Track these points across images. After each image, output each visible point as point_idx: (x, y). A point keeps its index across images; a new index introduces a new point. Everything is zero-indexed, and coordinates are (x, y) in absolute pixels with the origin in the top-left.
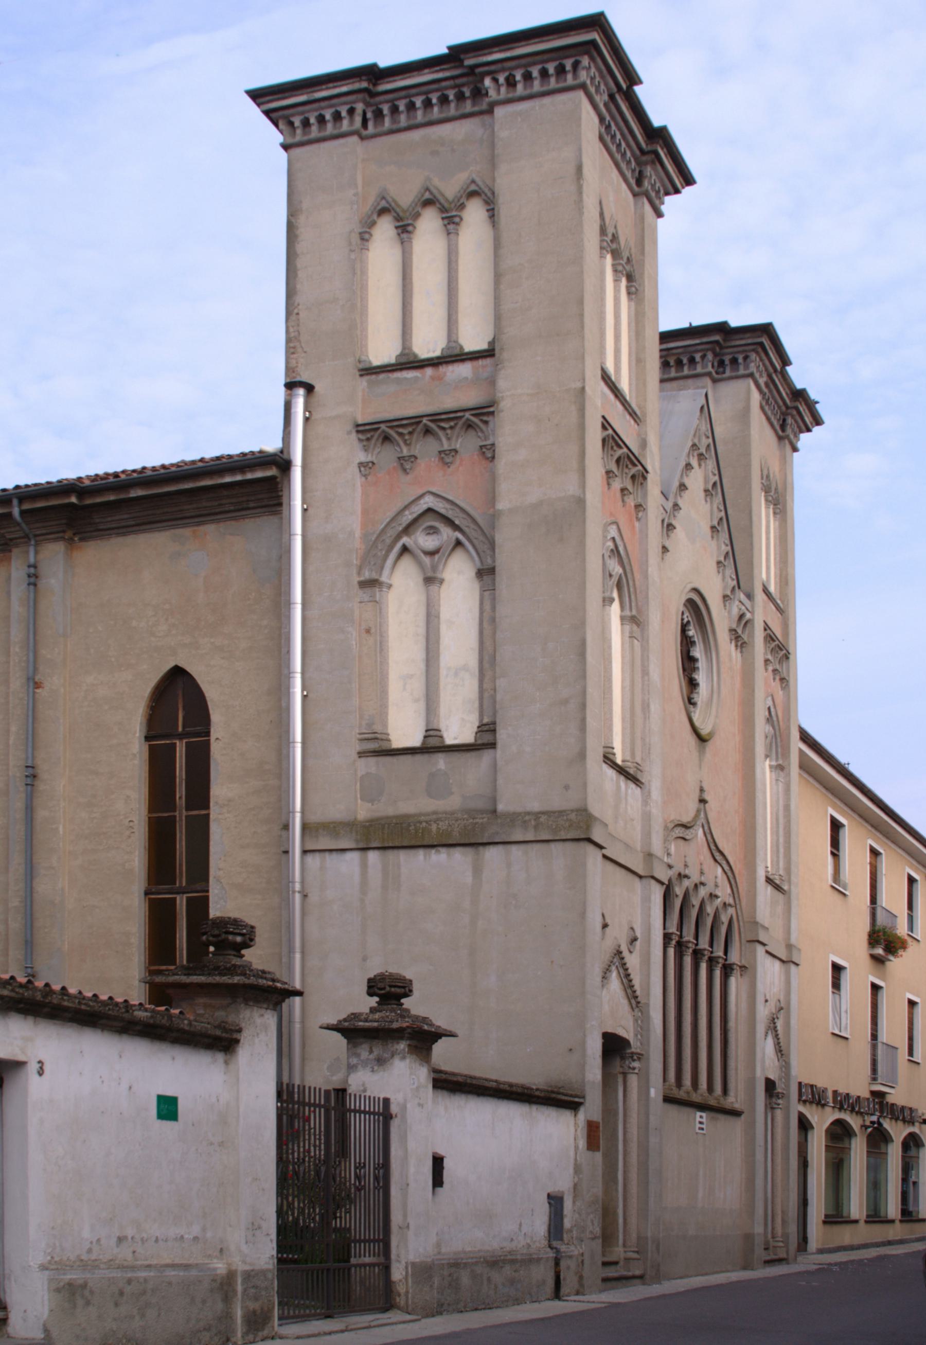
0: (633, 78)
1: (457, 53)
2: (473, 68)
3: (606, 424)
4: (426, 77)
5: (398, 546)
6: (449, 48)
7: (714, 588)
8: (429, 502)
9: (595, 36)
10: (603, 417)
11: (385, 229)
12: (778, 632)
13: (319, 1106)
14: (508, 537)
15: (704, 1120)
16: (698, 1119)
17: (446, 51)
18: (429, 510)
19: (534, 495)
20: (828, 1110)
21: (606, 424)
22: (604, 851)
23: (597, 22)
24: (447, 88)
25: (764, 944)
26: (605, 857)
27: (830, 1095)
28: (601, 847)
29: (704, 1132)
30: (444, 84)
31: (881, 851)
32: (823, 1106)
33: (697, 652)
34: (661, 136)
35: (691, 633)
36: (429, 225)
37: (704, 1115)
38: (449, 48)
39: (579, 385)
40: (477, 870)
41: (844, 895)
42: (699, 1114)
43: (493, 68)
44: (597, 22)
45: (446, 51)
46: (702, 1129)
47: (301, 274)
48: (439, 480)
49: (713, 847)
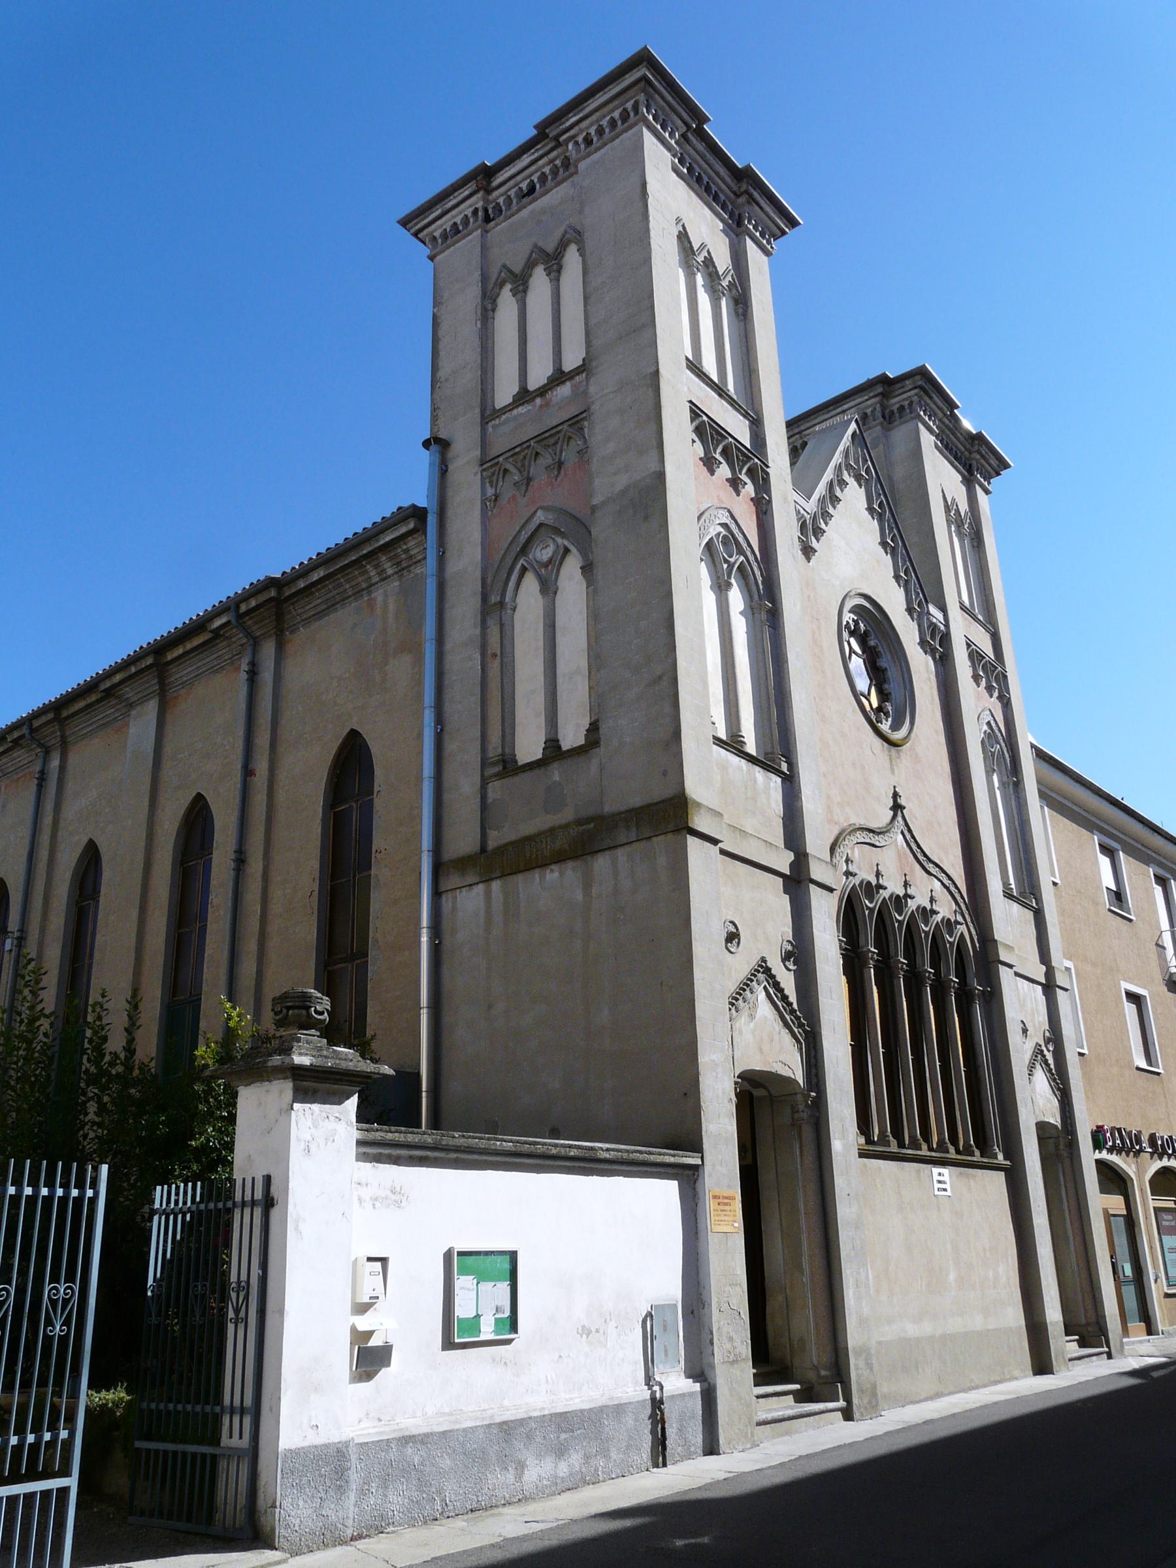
0: (702, 119)
1: (543, 128)
2: (556, 138)
3: (695, 412)
4: (526, 160)
5: (518, 567)
6: (536, 127)
7: (894, 602)
8: (540, 517)
9: (643, 71)
10: (690, 402)
11: (506, 294)
12: (987, 648)
13: (254, 1203)
14: (601, 528)
15: (946, 1178)
16: (936, 1177)
17: (535, 132)
18: (541, 525)
19: (622, 481)
20: (1145, 1156)
21: (695, 412)
22: (720, 845)
23: (644, 58)
24: (543, 166)
25: (1011, 966)
26: (723, 852)
27: (1145, 1138)
28: (715, 842)
29: (949, 1193)
30: (541, 163)
31: (1168, 876)
32: (1137, 1154)
33: (883, 663)
34: (745, 176)
35: (872, 643)
36: (539, 280)
37: (945, 1171)
38: (536, 127)
39: (653, 369)
40: (587, 886)
41: (1130, 920)
42: (936, 1170)
43: (572, 132)
44: (644, 58)
45: (535, 132)
46: (945, 1190)
47: (442, 353)
48: (549, 496)
49: (921, 858)
